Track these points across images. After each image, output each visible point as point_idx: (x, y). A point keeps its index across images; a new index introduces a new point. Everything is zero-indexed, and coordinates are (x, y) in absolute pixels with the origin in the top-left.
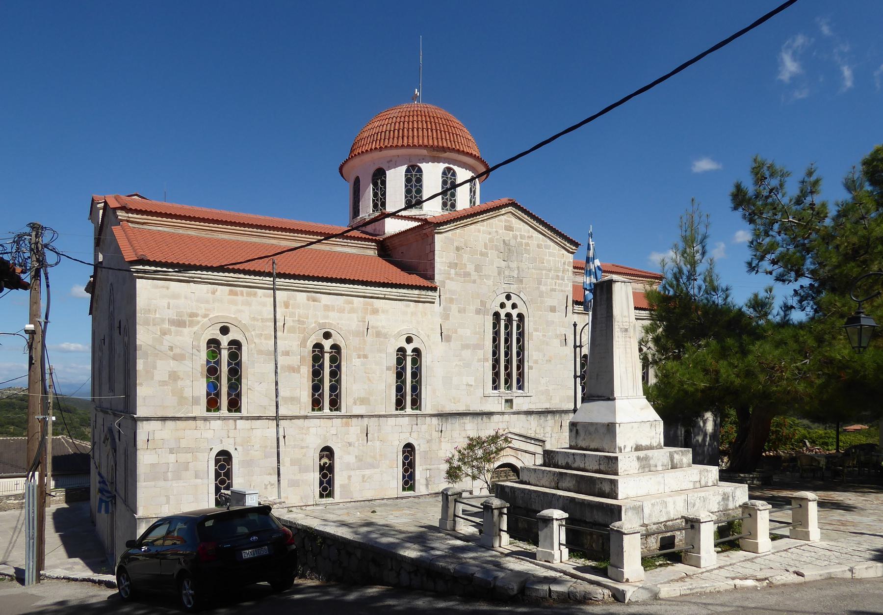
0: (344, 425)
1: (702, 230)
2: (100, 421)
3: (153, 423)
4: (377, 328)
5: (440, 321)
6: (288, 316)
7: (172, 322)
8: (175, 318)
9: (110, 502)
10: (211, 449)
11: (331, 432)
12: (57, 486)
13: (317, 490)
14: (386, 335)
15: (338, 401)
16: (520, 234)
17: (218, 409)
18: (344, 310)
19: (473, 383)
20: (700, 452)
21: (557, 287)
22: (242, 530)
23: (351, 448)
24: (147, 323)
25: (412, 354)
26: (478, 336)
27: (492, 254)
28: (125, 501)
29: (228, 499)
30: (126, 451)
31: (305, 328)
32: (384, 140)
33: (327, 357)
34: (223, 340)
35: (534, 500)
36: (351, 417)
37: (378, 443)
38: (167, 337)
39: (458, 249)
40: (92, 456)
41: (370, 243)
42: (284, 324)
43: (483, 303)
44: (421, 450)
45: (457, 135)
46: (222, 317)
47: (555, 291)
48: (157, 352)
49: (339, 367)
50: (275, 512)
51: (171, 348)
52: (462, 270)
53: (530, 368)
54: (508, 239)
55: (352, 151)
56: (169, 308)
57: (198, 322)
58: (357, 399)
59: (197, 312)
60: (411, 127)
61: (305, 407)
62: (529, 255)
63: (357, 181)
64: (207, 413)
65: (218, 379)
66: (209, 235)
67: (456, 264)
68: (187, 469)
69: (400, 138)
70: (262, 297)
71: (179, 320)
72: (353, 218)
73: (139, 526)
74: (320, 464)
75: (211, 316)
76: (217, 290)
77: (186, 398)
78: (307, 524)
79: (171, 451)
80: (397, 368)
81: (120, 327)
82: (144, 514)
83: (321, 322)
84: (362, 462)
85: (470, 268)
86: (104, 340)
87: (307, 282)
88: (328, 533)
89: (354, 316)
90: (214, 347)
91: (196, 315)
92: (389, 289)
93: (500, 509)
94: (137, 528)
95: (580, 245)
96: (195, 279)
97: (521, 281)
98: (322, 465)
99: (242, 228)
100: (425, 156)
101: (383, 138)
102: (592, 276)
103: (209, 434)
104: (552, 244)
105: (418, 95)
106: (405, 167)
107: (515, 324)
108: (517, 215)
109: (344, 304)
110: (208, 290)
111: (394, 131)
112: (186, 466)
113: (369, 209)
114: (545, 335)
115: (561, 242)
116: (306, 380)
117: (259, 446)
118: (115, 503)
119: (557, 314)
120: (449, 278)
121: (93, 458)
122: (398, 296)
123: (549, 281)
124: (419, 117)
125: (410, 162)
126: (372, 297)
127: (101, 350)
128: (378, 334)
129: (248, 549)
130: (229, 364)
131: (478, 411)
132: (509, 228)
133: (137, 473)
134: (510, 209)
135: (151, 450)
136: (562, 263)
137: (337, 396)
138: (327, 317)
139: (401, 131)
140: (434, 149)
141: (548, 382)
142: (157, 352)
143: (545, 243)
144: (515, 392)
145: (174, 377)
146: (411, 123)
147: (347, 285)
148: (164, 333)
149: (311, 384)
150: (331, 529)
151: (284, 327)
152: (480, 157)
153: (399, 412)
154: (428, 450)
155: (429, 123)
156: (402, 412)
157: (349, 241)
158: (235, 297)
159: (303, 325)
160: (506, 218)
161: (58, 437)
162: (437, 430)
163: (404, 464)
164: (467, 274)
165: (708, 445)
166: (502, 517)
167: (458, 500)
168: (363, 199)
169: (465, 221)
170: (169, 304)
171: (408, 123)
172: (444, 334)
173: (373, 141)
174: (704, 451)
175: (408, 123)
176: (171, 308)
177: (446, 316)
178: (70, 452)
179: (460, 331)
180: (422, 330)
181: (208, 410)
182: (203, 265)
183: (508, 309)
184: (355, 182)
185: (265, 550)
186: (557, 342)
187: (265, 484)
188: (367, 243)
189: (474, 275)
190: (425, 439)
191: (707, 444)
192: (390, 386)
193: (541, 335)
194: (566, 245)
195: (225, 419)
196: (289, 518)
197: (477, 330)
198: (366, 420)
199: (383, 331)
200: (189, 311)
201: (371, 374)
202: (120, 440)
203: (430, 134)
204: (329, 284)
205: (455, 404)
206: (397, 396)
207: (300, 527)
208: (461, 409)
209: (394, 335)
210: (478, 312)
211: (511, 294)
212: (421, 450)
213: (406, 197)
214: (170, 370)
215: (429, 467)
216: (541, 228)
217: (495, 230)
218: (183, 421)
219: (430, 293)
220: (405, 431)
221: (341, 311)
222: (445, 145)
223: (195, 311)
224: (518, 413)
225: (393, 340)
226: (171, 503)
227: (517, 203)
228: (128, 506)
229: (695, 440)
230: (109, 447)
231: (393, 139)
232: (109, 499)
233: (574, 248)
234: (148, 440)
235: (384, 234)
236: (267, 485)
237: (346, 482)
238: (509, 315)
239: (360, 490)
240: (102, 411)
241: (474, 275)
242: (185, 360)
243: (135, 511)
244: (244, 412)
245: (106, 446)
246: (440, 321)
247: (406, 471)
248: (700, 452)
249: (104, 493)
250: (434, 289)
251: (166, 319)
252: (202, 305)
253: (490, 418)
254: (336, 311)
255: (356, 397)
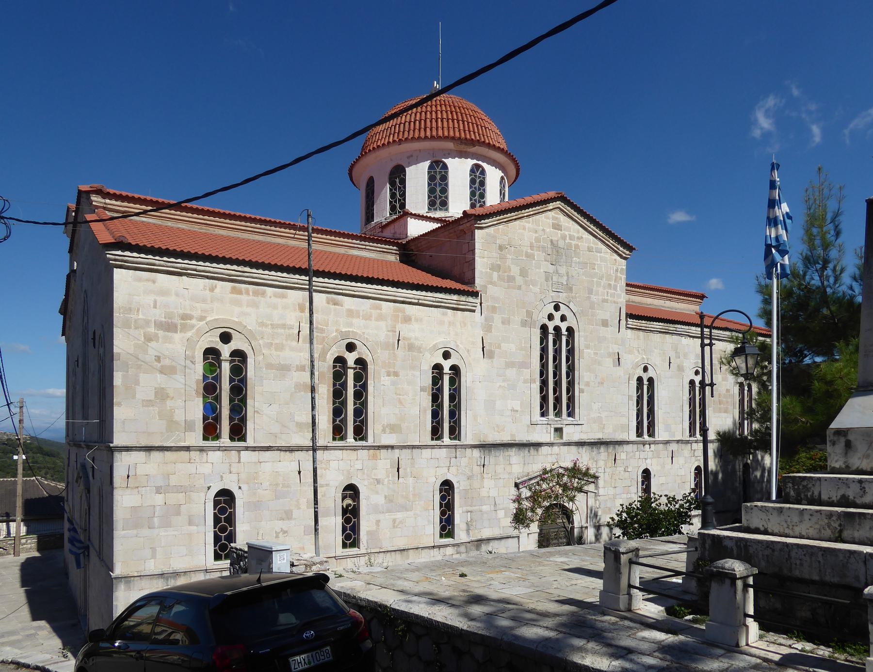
0: (370, 458)
1: (832, 206)
2: (73, 458)
3: (134, 454)
4: (409, 339)
5: (481, 333)
6: (304, 322)
7: (160, 325)
8: (164, 320)
9: (82, 555)
10: (209, 488)
11: (355, 466)
12: (28, 532)
13: (340, 538)
14: (420, 348)
15: (363, 429)
16: (569, 234)
17: (218, 437)
18: (371, 316)
19: (518, 408)
20: (759, 489)
21: (609, 298)
22: (286, 619)
23: (380, 486)
24: (127, 325)
25: (450, 372)
26: (524, 352)
27: (539, 255)
28: (100, 554)
29: (242, 556)
30: (100, 491)
31: (324, 337)
32: (403, 132)
33: (351, 373)
34: (224, 349)
35: (798, 562)
36: (379, 447)
37: (411, 480)
38: (153, 344)
39: (501, 248)
40: (66, 498)
41: (391, 247)
42: (299, 332)
43: (529, 314)
44: (461, 488)
45: (485, 128)
46: (223, 320)
47: (608, 303)
48: (140, 363)
49: (365, 387)
50: (335, 585)
51: (158, 359)
52: (506, 274)
53: (581, 391)
54: (556, 239)
55: (363, 149)
56: (155, 307)
57: (193, 326)
58: (387, 427)
59: (192, 313)
60: (434, 117)
61: (325, 436)
62: (579, 258)
63: (371, 182)
64: (204, 442)
65: (218, 399)
66: (204, 230)
67: (499, 267)
68: (178, 513)
69: (422, 130)
70: (273, 298)
71: (168, 323)
72: (366, 224)
73: (117, 587)
74: (342, 505)
75: (208, 319)
76: (216, 287)
77: (177, 423)
78: (376, 600)
79: (158, 490)
80: (433, 389)
81: (94, 339)
82: (123, 571)
83: (343, 330)
84: (392, 504)
85: (515, 271)
86: (78, 361)
87: (326, 280)
88: (417, 616)
89: (382, 324)
90: (213, 359)
91: (190, 317)
92: (424, 293)
93: (744, 578)
94: (114, 590)
95: (635, 249)
96: (189, 271)
97: (571, 289)
98: (345, 507)
99: (243, 223)
100: (451, 150)
101: (402, 130)
102: (780, 226)
103: (206, 469)
104: (604, 247)
105: (438, 87)
106: (427, 164)
107: (564, 339)
108: (566, 211)
109: (370, 309)
110: (205, 286)
111: (415, 123)
112: (177, 510)
113: (385, 213)
114: (597, 354)
115: (613, 245)
116: (326, 401)
117: (268, 483)
118: (88, 555)
119: (609, 329)
120: (492, 283)
121: (67, 501)
122: (434, 302)
123: (601, 289)
124: (443, 106)
125: (434, 157)
126: (403, 302)
127: (75, 374)
128: (411, 347)
129: (299, 654)
130: (231, 380)
131: (525, 442)
132: (557, 227)
133: (114, 519)
134: (558, 204)
135: (132, 488)
136: (614, 270)
137: (362, 422)
138: (351, 325)
139: (423, 122)
140: (461, 142)
141: (601, 408)
142: (140, 363)
143: (596, 246)
144: (565, 420)
145: (162, 395)
146: (434, 113)
147: (375, 286)
148: (149, 339)
149: (331, 407)
150: (421, 609)
151: (299, 335)
152: (511, 154)
153: (434, 443)
154: (469, 488)
155: (454, 113)
156: (438, 442)
157: (367, 243)
158: (238, 296)
159: (322, 333)
160: (554, 215)
161: (32, 479)
162: (479, 464)
163: (441, 505)
164: (511, 279)
165: (767, 481)
166: (747, 591)
167: (634, 559)
168: (378, 202)
169: (509, 215)
170: (155, 302)
171: (431, 113)
172: (486, 350)
173: (390, 134)
174: (762, 489)
175: (431, 113)
176: (158, 307)
177: (488, 328)
178: (44, 494)
179: (504, 346)
180: (460, 344)
181: (205, 438)
182: (199, 253)
183: (557, 321)
184: (368, 183)
185: (326, 654)
186: (609, 362)
187: (276, 532)
188: (387, 247)
189: (519, 280)
190: (465, 474)
191: (765, 480)
192: (425, 411)
193: (592, 354)
194: (618, 249)
195: (226, 449)
196: (342, 587)
197: (523, 345)
198: (397, 451)
199: (417, 343)
200: (181, 312)
201: (403, 395)
202: (94, 479)
203: (456, 126)
204: (353, 284)
205: (499, 432)
206: (432, 422)
207: (364, 604)
208: (506, 438)
209: (430, 349)
210: (524, 324)
211: (559, 304)
212: (461, 488)
213: (429, 197)
214: (157, 386)
215: (469, 508)
216: (592, 228)
217: (541, 228)
218: (173, 452)
219: (470, 299)
220: (442, 465)
221: (368, 317)
222: (473, 137)
223: (188, 312)
224: (569, 444)
225: (427, 355)
226: (157, 557)
227: (566, 197)
228: (103, 560)
229: (753, 475)
230: (82, 487)
231: (414, 131)
232: (81, 551)
233: (628, 252)
234: (128, 476)
235: (407, 237)
236: (279, 533)
237: (374, 528)
238: (557, 329)
239: (390, 538)
240: (75, 445)
241: (519, 280)
242: (176, 374)
243: (111, 568)
244: (250, 442)
245: (79, 486)
246: (481, 333)
247: (443, 513)
248: (759, 489)
249: (75, 543)
250: (475, 294)
251: (151, 321)
252: (197, 305)
253: (537, 450)
254: (361, 318)
255: (386, 424)
